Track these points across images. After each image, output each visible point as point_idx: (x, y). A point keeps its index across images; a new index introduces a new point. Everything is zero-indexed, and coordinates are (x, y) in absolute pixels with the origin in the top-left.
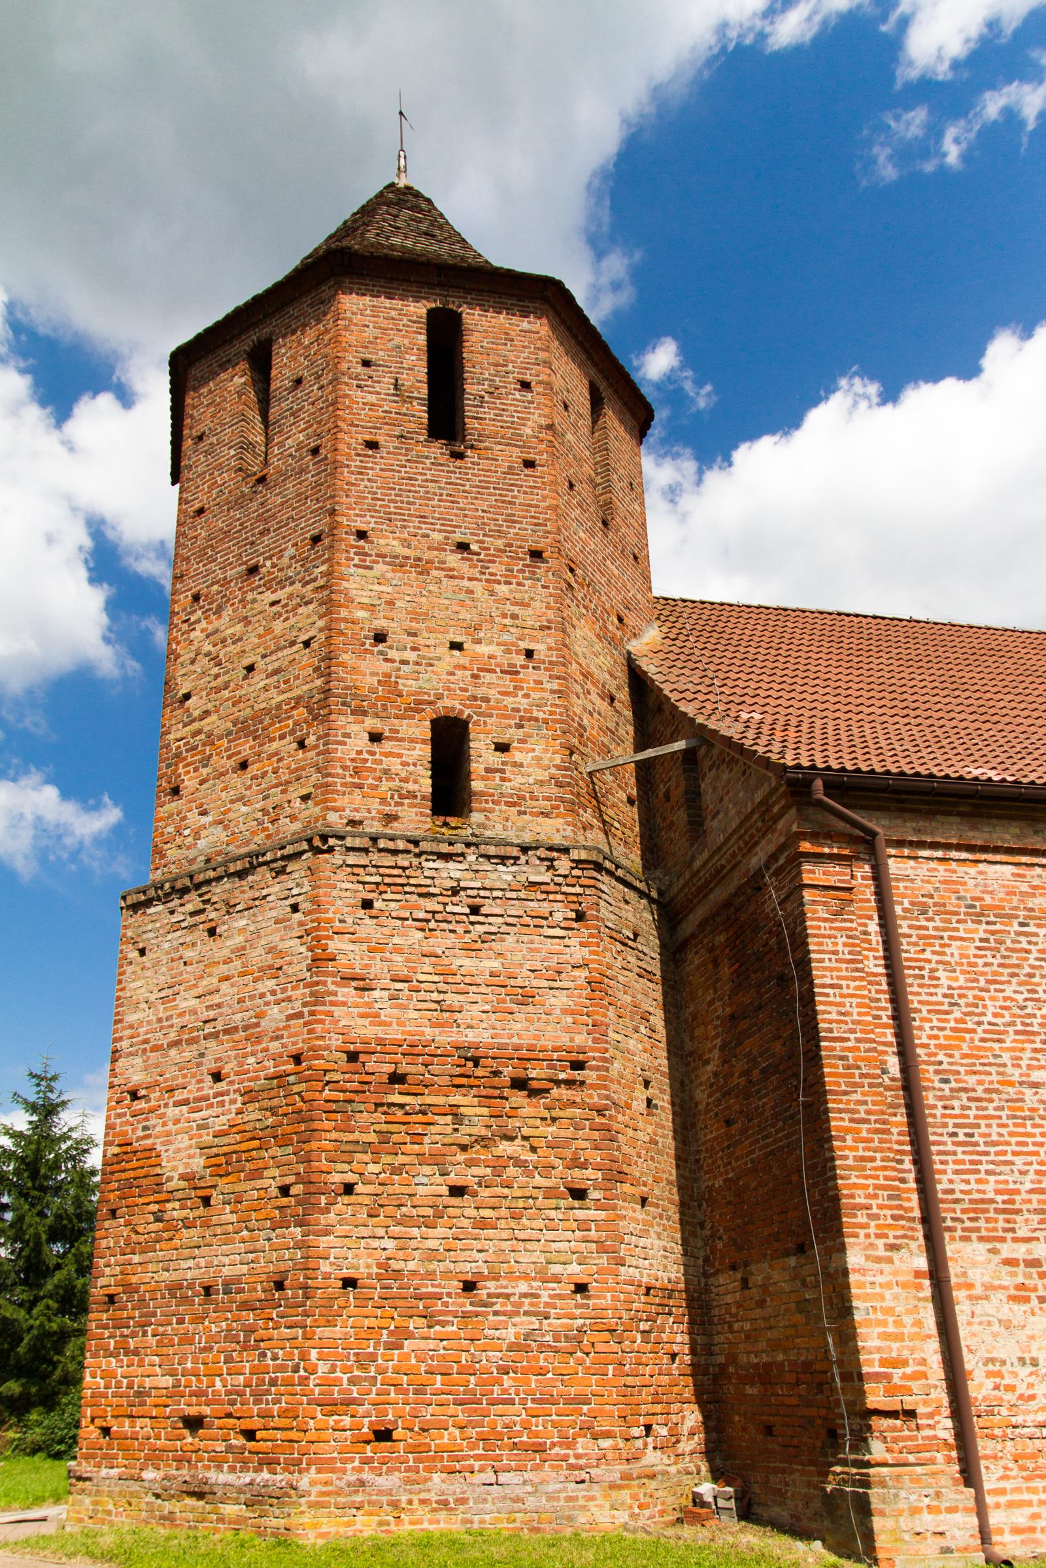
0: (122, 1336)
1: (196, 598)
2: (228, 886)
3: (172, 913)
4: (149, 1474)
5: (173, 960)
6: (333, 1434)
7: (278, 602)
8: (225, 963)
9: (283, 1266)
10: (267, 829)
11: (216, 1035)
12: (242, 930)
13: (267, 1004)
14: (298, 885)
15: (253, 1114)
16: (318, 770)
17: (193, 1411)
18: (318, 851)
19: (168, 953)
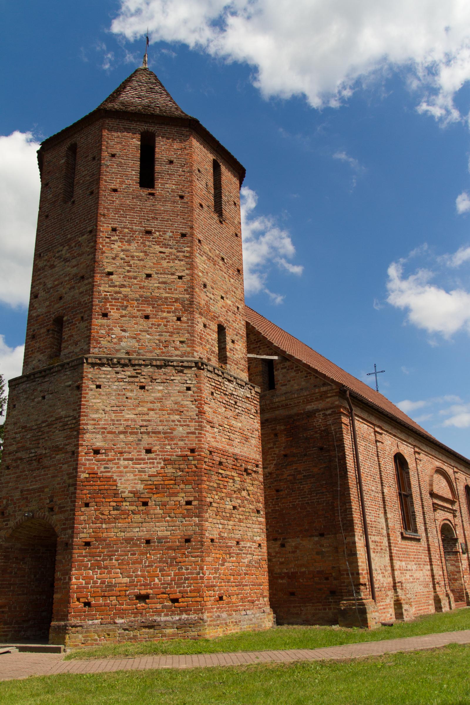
0: (97, 560)
1: (114, 230)
2: (151, 370)
3: (117, 373)
4: (119, 621)
5: (119, 395)
6: (210, 597)
7: (164, 253)
8: (151, 403)
9: (190, 533)
10: (162, 349)
11: (148, 433)
12: (159, 391)
13: (177, 425)
14: (190, 380)
15: (170, 470)
16: (189, 333)
17: (143, 592)
18: (199, 368)
19: (115, 391)
